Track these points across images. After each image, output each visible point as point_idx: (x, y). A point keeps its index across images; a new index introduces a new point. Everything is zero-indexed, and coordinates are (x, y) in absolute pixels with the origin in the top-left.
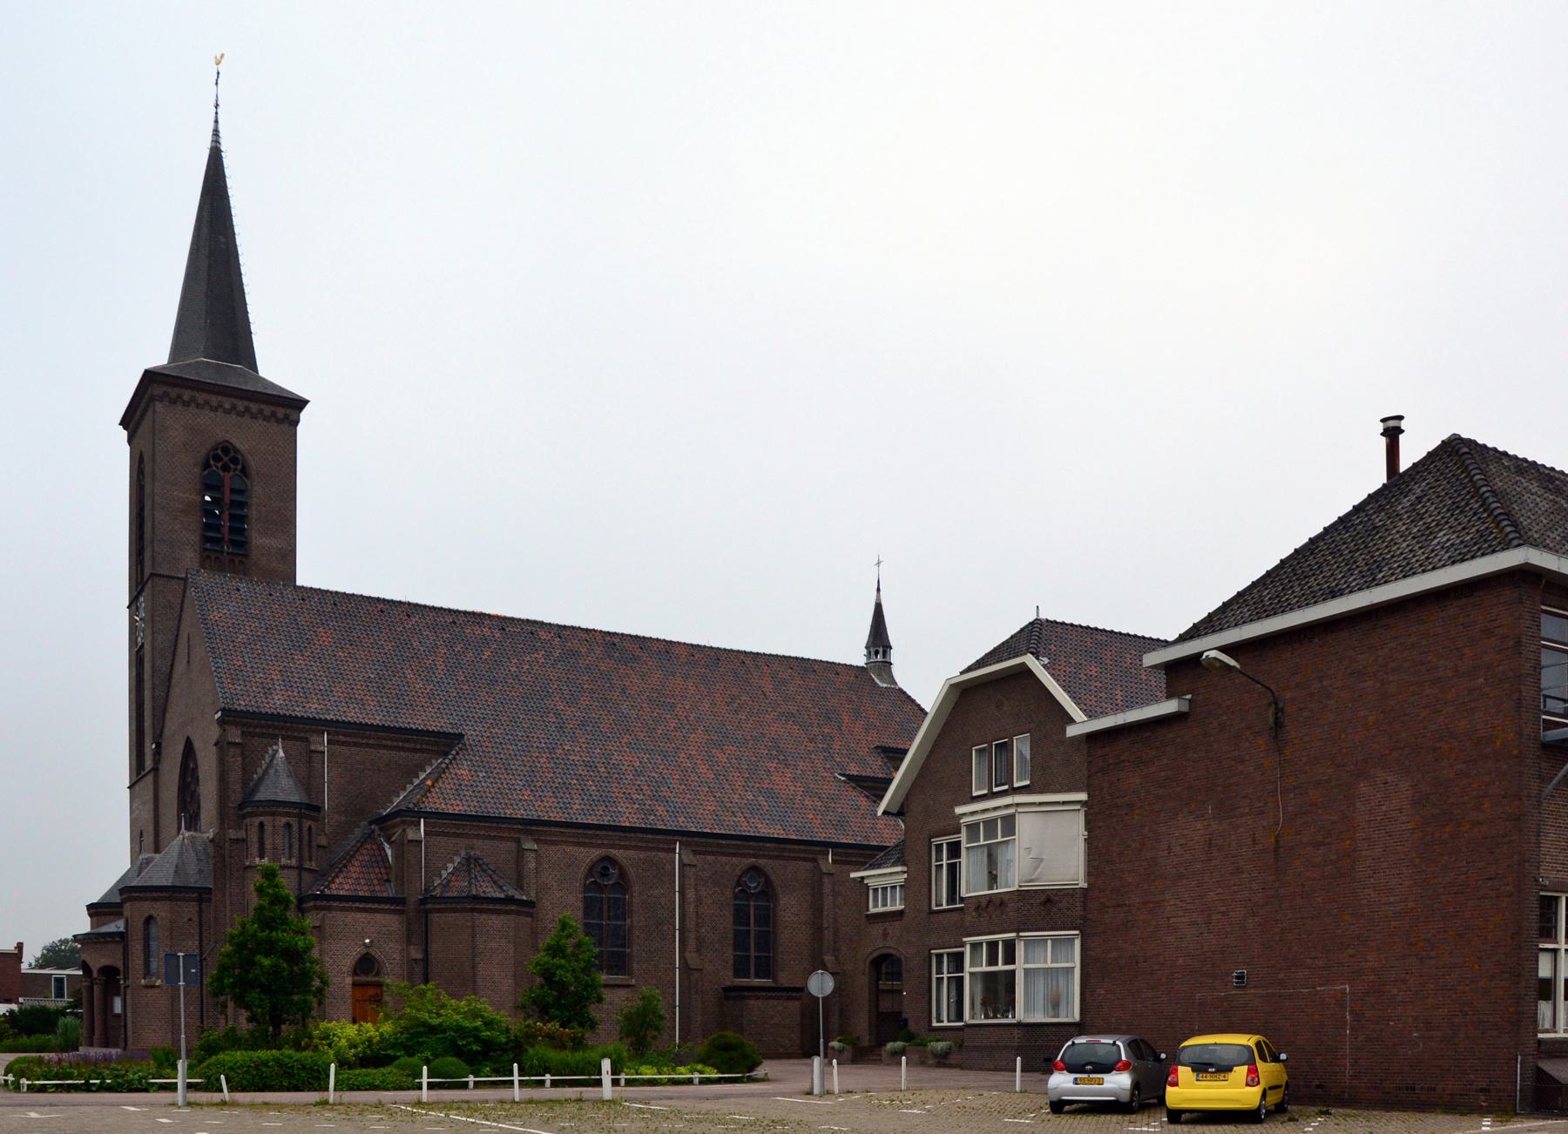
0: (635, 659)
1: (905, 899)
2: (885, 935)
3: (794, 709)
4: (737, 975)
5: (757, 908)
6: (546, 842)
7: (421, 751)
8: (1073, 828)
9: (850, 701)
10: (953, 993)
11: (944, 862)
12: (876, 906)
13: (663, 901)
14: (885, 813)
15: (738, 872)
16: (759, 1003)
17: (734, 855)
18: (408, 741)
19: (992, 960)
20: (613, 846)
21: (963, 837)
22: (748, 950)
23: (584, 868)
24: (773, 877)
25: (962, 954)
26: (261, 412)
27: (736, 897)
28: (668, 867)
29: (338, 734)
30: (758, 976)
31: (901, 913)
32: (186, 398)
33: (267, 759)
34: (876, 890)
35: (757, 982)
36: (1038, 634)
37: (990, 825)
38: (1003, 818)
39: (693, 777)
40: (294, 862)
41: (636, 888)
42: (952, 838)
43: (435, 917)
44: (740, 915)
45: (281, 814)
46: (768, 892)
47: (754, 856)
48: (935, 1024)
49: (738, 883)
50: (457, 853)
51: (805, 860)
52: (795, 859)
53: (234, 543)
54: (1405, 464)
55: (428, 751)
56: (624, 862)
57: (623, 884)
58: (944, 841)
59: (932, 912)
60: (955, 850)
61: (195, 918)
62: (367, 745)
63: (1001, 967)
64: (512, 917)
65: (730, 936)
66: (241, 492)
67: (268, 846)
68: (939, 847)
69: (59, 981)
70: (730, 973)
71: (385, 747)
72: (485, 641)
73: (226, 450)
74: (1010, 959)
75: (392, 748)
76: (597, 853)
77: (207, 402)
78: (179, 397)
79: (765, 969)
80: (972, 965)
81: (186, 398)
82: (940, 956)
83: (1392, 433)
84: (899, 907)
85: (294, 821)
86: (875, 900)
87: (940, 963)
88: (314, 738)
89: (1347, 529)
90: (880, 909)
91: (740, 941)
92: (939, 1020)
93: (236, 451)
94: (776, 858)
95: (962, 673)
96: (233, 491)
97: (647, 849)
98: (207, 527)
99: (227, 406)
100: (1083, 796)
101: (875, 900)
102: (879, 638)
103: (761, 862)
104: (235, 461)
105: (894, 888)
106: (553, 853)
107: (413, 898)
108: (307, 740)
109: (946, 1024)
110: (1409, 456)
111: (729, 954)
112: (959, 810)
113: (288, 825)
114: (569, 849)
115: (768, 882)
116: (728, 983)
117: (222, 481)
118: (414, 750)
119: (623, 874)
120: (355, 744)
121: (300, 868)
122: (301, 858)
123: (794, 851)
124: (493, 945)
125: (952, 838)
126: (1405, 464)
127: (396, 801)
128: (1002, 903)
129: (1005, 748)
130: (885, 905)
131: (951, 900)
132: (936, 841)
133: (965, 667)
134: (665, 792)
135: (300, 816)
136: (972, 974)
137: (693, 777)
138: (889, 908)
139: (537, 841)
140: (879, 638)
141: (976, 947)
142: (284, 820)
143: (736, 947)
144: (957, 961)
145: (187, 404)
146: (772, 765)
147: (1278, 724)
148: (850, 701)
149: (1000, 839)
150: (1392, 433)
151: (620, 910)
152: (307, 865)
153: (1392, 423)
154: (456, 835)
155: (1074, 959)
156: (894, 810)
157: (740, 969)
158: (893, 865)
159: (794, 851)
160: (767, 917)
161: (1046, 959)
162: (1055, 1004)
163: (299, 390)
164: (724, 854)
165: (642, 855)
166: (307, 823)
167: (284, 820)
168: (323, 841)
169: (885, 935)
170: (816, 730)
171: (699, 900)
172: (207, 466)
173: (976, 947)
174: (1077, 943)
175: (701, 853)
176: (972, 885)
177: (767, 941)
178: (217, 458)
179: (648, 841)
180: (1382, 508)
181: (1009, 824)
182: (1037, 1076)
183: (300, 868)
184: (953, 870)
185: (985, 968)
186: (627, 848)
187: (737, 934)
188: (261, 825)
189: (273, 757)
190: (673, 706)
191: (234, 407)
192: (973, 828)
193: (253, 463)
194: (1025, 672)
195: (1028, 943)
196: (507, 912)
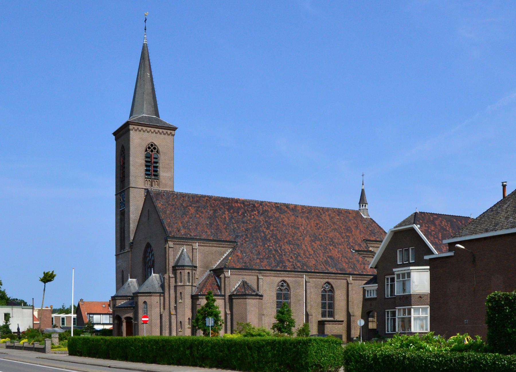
0: (286, 212)
1: (377, 294)
2: (371, 305)
3: (337, 227)
4: (322, 317)
5: (329, 295)
6: (265, 276)
7: (225, 247)
9: (354, 223)
10: (392, 323)
11: (389, 283)
15: (323, 284)
16: (330, 325)
17: (321, 278)
19: (404, 313)
21: (396, 276)
22: (326, 308)
23: (276, 284)
24: (333, 286)
25: (395, 311)
26: (163, 132)
27: (322, 292)
28: (302, 283)
30: (329, 317)
31: (375, 299)
32: (140, 129)
33: (180, 251)
34: (368, 291)
35: (328, 319)
36: (417, 217)
37: (403, 275)
39: (307, 253)
40: (190, 284)
41: (292, 290)
42: (392, 276)
43: (234, 300)
44: (323, 297)
46: (332, 290)
47: (328, 278)
48: (387, 332)
49: (323, 287)
53: (155, 175)
54: (507, 194)
56: (288, 282)
57: (288, 289)
59: (385, 298)
60: (393, 280)
61: (159, 302)
62: (209, 246)
63: (407, 316)
64: (257, 300)
65: (320, 304)
66: (157, 158)
68: (388, 279)
70: (321, 316)
71: (214, 246)
72: (239, 208)
74: (410, 313)
75: (216, 247)
76: (281, 279)
78: (138, 129)
79: (331, 314)
80: (398, 315)
81: (140, 129)
82: (388, 312)
83: (504, 186)
84: (375, 296)
85: (190, 271)
86: (368, 294)
87: (388, 314)
88: (194, 244)
89: (492, 211)
90: (369, 297)
91: (323, 306)
92: (388, 331)
95: (394, 228)
96: (154, 158)
97: (296, 277)
98: (146, 170)
99: (152, 131)
100: (428, 267)
101: (368, 294)
102: (362, 200)
103: (330, 280)
104: (155, 148)
105: (373, 290)
106: (268, 279)
107: (228, 294)
108: (192, 245)
109: (390, 332)
110: (508, 192)
112: (394, 270)
113: (189, 273)
114: (272, 278)
115: (332, 287)
117: (151, 155)
118: (223, 247)
121: (192, 286)
122: (192, 283)
123: (340, 277)
125: (392, 276)
126: (507, 194)
127: (218, 263)
129: (408, 250)
130: (371, 295)
131: (391, 295)
132: (387, 277)
133: (395, 226)
135: (192, 270)
136: (398, 318)
137: (307, 253)
138: (372, 296)
139: (263, 276)
140: (362, 200)
141: (399, 309)
142: (188, 271)
143: (322, 308)
144: (394, 314)
145: (140, 131)
146: (331, 247)
148: (354, 223)
149: (406, 279)
150: (504, 186)
151: (287, 297)
152: (194, 284)
153: (505, 184)
156: (374, 267)
157: (323, 315)
158: (373, 284)
159: (340, 277)
160: (332, 298)
161: (421, 315)
163: (175, 126)
164: (318, 278)
165: (294, 279)
166: (194, 272)
167: (188, 271)
170: (344, 234)
171: (311, 292)
172: (146, 151)
173: (399, 309)
174: (429, 310)
176: (398, 291)
177: (331, 306)
178: (149, 148)
179: (295, 275)
180: (500, 207)
181: (409, 275)
182: (413, 300)
183: (192, 286)
184: (392, 287)
185: (402, 316)
186: (289, 277)
187: (322, 304)
188: (181, 272)
189: (182, 251)
190: (298, 228)
192: (398, 276)
193: (160, 150)
194: (413, 230)
195: (414, 309)
196: (257, 299)
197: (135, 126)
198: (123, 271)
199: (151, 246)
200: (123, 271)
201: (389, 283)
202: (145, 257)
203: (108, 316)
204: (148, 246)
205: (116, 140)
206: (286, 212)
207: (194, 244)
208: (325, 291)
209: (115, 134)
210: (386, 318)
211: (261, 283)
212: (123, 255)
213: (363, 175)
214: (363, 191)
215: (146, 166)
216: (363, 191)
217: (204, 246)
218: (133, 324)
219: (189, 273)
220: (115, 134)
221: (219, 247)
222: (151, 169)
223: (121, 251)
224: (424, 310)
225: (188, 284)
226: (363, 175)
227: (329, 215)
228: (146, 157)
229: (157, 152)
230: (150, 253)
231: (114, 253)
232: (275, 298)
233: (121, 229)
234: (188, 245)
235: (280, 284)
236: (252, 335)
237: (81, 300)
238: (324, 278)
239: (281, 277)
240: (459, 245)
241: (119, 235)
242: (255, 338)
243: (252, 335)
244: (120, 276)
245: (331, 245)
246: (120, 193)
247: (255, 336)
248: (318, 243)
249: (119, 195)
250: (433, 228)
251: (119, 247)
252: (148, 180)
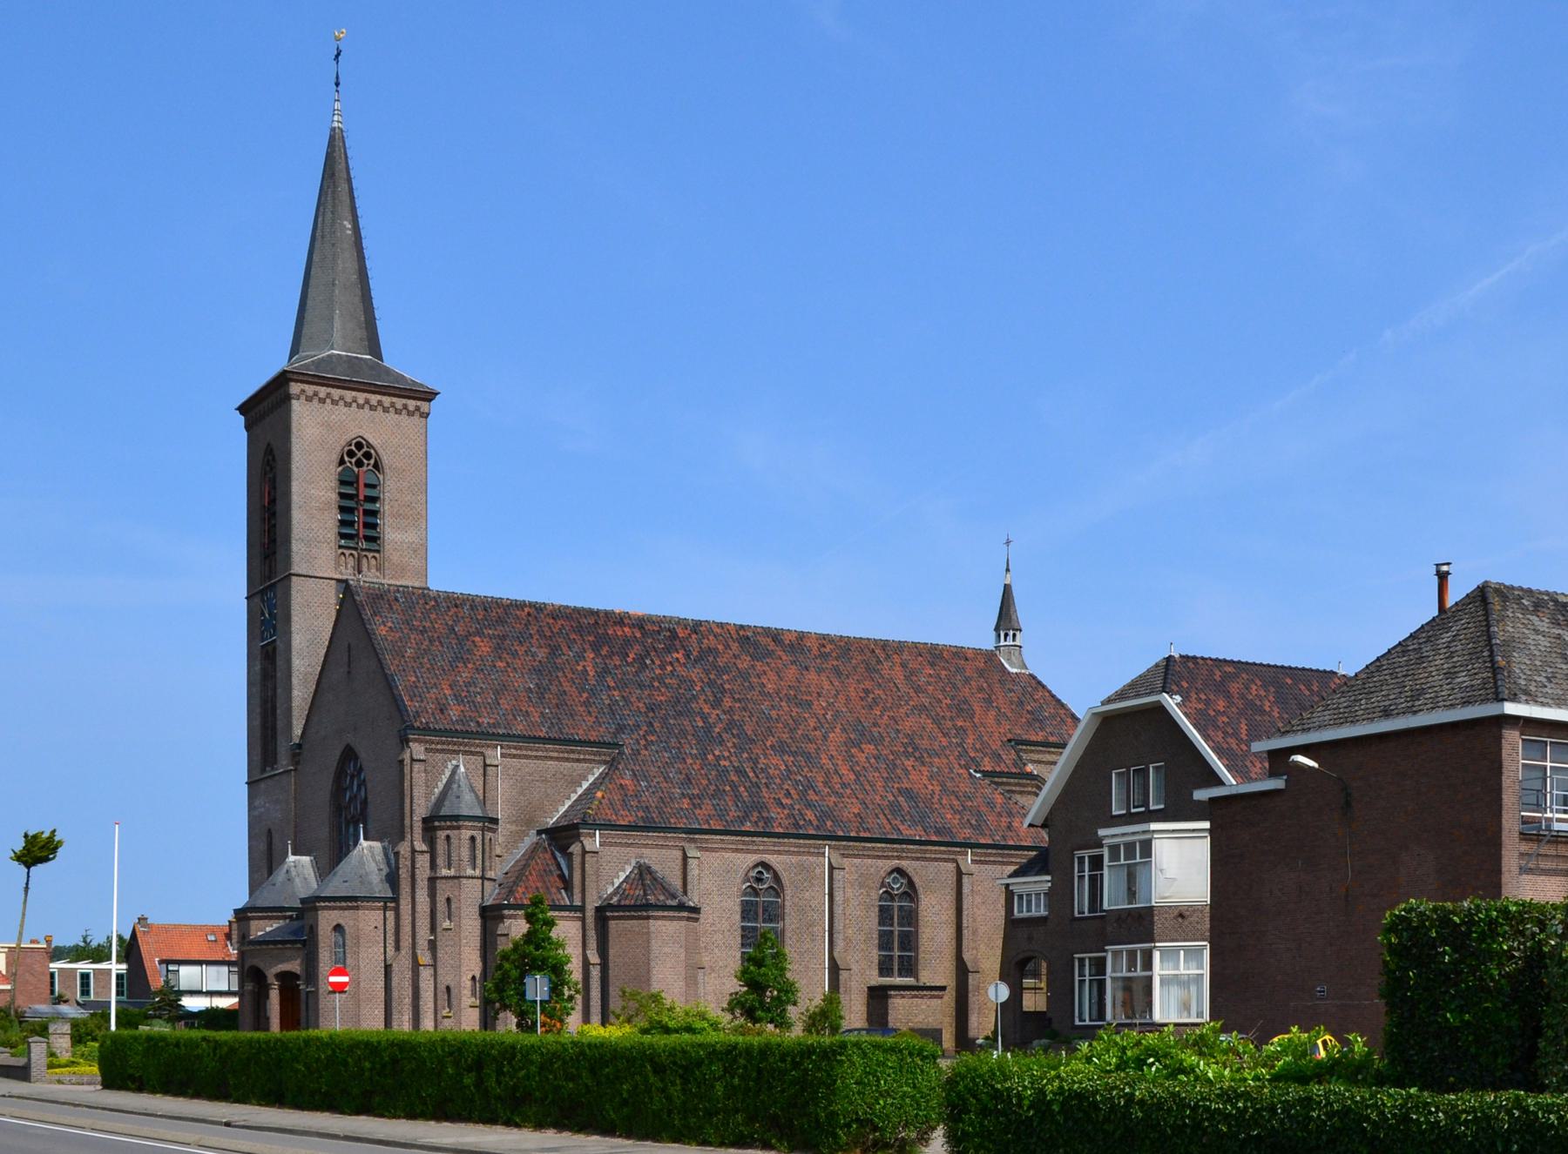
0: (770, 654)
1: (1049, 906)
2: (1030, 939)
4: (881, 974)
6: (707, 849)
7: (585, 761)
8: (1201, 850)
11: (1086, 874)
12: (1020, 911)
13: (814, 903)
14: (1031, 825)
15: (883, 874)
17: (879, 857)
18: (573, 752)
19: (1132, 965)
20: (764, 852)
21: (1106, 852)
22: (891, 949)
23: (741, 873)
24: (916, 880)
25: (1104, 959)
28: (818, 871)
29: (509, 747)
30: (900, 975)
31: (1043, 920)
33: (448, 773)
34: (1021, 897)
35: (898, 981)
36: (1172, 672)
37: (1130, 847)
38: (1142, 842)
39: (836, 779)
40: (478, 873)
41: (788, 892)
42: (1095, 852)
43: (612, 923)
44: (885, 915)
45: (467, 828)
46: (911, 893)
47: (899, 858)
48: (1077, 1023)
49: (883, 885)
50: (627, 862)
51: (946, 860)
52: (936, 860)
54: (1450, 601)
55: (590, 761)
56: (778, 867)
57: (777, 888)
58: (1086, 853)
60: (1097, 862)
63: (1139, 972)
64: (683, 923)
65: (875, 936)
66: (374, 487)
67: (454, 858)
68: (1081, 860)
69: (85, 977)
70: (876, 972)
71: (551, 758)
73: (359, 446)
74: (1148, 965)
75: (557, 759)
76: (753, 858)
77: (341, 398)
78: (316, 394)
79: (909, 967)
80: (1114, 971)
81: (322, 395)
82: (1082, 961)
83: (1443, 577)
84: (1043, 912)
85: (478, 834)
86: (1020, 905)
87: (1082, 966)
88: (489, 752)
90: (1025, 914)
91: (885, 942)
93: (369, 445)
94: (918, 859)
95: (1103, 703)
96: (367, 485)
97: (799, 853)
98: (343, 523)
99: (361, 401)
102: (1006, 620)
103: (904, 864)
104: (368, 456)
108: (482, 754)
109: (1087, 1023)
110: (1454, 596)
111: (875, 954)
112: (1101, 832)
113: (473, 839)
114: (727, 855)
115: (911, 883)
116: (873, 983)
117: (357, 477)
119: (777, 878)
120: (526, 757)
121: (483, 878)
123: (936, 852)
124: (667, 950)
125: (1095, 852)
126: (1450, 601)
127: (562, 810)
128: (1140, 916)
130: (1029, 910)
132: (1079, 853)
134: (812, 796)
137: (836, 779)
138: (1034, 913)
139: (701, 849)
140: (1006, 620)
141: (1116, 954)
142: (470, 833)
143: (881, 947)
144: (1099, 966)
146: (908, 763)
147: (1348, 804)
150: (1443, 577)
151: (774, 913)
153: (1445, 568)
154: (629, 845)
155: (1203, 969)
156: (1039, 822)
157: (885, 969)
158: (1036, 874)
159: (936, 852)
160: (911, 918)
162: (1185, 1007)
164: (869, 857)
167: (470, 833)
168: (498, 851)
169: (1030, 939)
171: (846, 901)
172: (342, 462)
175: (848, 856)
176: (1112, 898)
177: (909, 941)
178: (351, 454)
181: (1147, 848)
183: (483, 878)
185: (1125, 974)
186: (779, 853)
187: (882, 934)
188: (448, 837)
190: (809, 704)
191: (367, 401)
192: (1114, 850)
193: (386, 460)
194: (1160, 709)
195: (1163, 951)
196: (680, 919)
197: (306, 387)
198: (270, 831)
199: (356, 758)
200: (270, 831)
201: (1086, 874)
202: (338, 789)
203: (225, 969)
204: (349, 754)
205: (248, 427)
206: (770, 654)
207: (489, 752)
208: (889, 895)
209: (243, 409)
210: (1077, 978)
211: (696, 872)
212: (270, 782)
213: (1008, 543)
214: (1007, 589)
215: (342, 509)
216: (1007, 589)
217: (519, 757)
218: (303, 996)
219: (473, 839)
220: (243, 409)
221: (567, 760)
222: (359, 518)
223: (263, 771)
224: (1193, 954)
225: (470, 872)
226: (1008, 543)
227: (904, 665)
228: (342, 483)
229: (376, 466)
230: (352, 777)
231: (243, 776)
232: (738, 917)
233: (264, 702)
234: (472, 753)
235: (753, 874)
236: (667, 1030)
237: (142, 920)
238: (887, 857)
239: (755, 852)
240: (1300, 759)
241: (257, 723)
242: (674, 1036)
243: (667, 1030)
244: (263, 846)
245: (906, 754)
246: (262, 592)
247: (676, 1031)
248: (869, 748)
249: (257, 600)
250: (1221, 704)
251: (257, 758)
252: (347, 552)
